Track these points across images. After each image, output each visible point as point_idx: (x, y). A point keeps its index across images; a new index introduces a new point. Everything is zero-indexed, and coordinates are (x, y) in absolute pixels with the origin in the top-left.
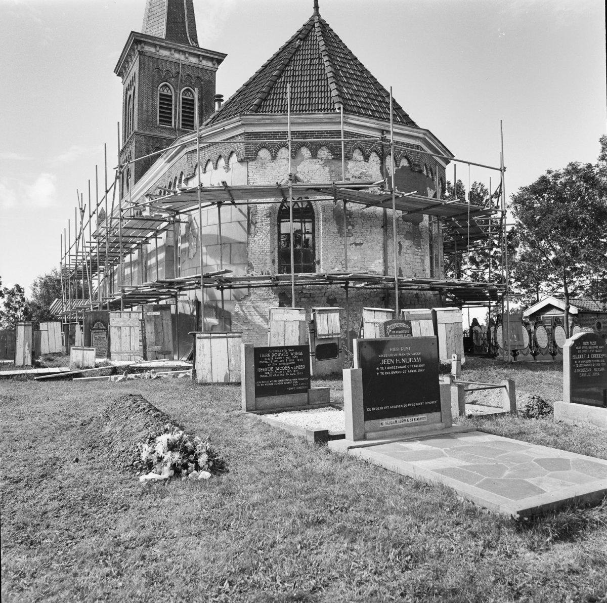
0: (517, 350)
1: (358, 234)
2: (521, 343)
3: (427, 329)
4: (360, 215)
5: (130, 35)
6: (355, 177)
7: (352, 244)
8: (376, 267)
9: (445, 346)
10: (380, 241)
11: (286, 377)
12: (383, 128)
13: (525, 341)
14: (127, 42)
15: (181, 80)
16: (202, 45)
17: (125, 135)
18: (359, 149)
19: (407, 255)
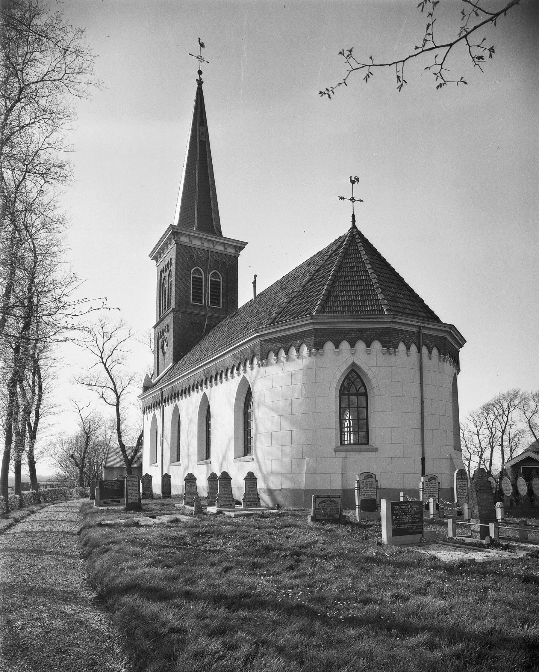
5: (169, 227)
11: (409, 523)
14: (166, 232)
15: (210, 265)
16: (224, 235)
17: (160, 310)
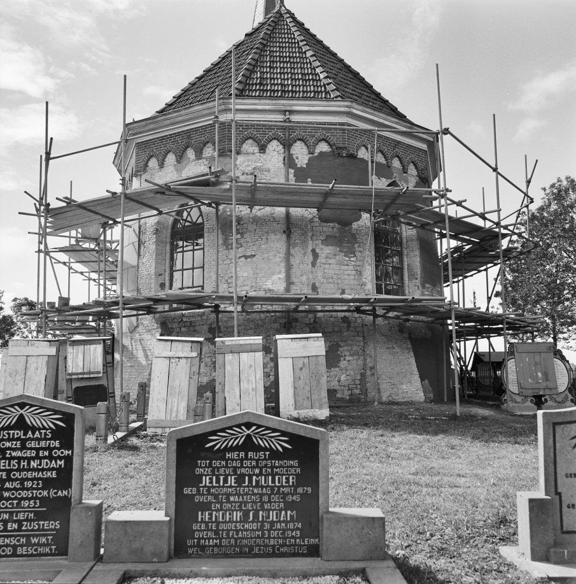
0: (544, 396)
1: (249, 245)
2: (550, 385)
3: (251, 366)
4: (251, 220)
6: (247, 174)
7: (241, 257)
8: (275, 284)
9: (291, 391)
10: (281, 250)
12: (283, 108)
13: (559, 382)
18: (398, 156)
19: (327, 266)
